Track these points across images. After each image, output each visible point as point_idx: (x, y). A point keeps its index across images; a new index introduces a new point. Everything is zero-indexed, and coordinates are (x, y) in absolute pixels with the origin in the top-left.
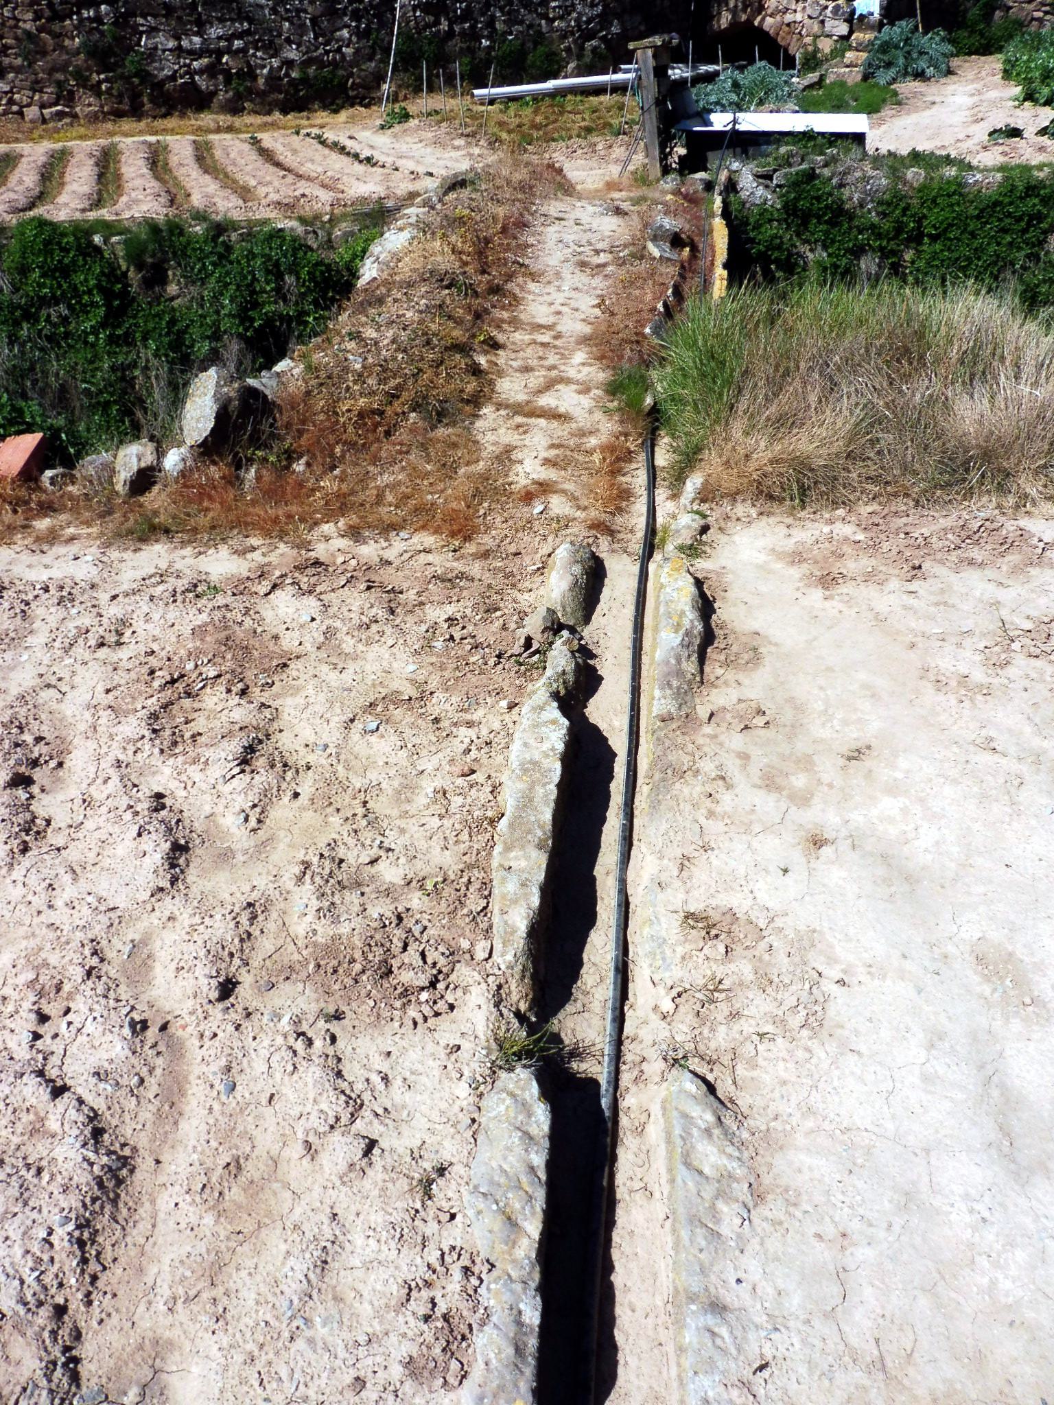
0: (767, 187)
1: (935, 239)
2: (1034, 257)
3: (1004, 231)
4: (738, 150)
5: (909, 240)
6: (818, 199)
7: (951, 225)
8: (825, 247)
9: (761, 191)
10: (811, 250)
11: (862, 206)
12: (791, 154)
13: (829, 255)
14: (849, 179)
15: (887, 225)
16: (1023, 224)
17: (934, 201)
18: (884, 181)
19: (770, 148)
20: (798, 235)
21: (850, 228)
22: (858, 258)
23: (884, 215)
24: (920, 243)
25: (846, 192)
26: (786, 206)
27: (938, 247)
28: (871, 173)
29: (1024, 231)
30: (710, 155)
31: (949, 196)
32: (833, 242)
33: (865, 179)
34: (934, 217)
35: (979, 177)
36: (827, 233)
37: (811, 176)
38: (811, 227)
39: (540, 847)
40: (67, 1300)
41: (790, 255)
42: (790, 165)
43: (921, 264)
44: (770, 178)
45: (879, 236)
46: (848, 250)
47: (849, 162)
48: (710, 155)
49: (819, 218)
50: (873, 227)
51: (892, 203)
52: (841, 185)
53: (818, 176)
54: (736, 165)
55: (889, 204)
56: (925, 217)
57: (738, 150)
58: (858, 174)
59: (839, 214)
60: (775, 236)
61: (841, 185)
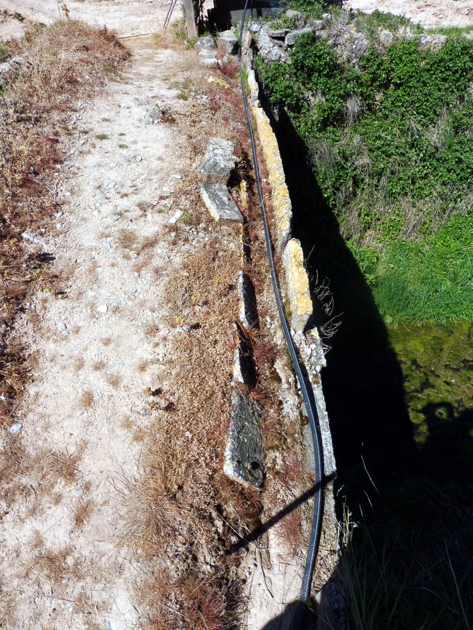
0: (280, 46)
1: (398, 86)
2: (462, 98)
3: (444, 80)
4: (255, 10)
5: (380, 86)
6: (320, 57)
7: (411, 77)
8: (324, 94)
9: (276, 51)
10: (313, 95)
11: (349, 61)
12: (296, 19)
13: (327, 100)
14: (341, 40)
15: (366, 77)
16: (458, 75)
17: (400, 59)
18: (365, 42)
19: (280, 10)
20: (304, 84)
21: (341, 79)
22: (345, 101)
23: (364, 68)
24: (387, 88)
25: (338, 50)
26: (295, 63)
27: (400, 92)
28: (356, 35)
29: (458, 80)
30: (233, 13)
31: (410, 54)
32: (330, 90)
33: (352, 40)
34: (400, 71)
35: (429, 38)
36: (325, 84)
37: (313, 39)
38: (314, 79)
39: (259, 107)
40: (83, 446)
41: (298, 100)
42: (296, 28)
43: (388, 104)
44: (282, 39)
45: (361, 85)
46: (340, 96)
47: (340, 26)
48: (233, 13)
49: (320, 72)
50: (358, 78)
51: (369, 59)
52: (335, 45)
53: (319, 38)
54: (255, 27)
55: (368, 60)
56: (393, 70)
57: (255, 10)
58: (347, 36)
59: (334, 69)
60: (287, 87)
61: (335, 45)
